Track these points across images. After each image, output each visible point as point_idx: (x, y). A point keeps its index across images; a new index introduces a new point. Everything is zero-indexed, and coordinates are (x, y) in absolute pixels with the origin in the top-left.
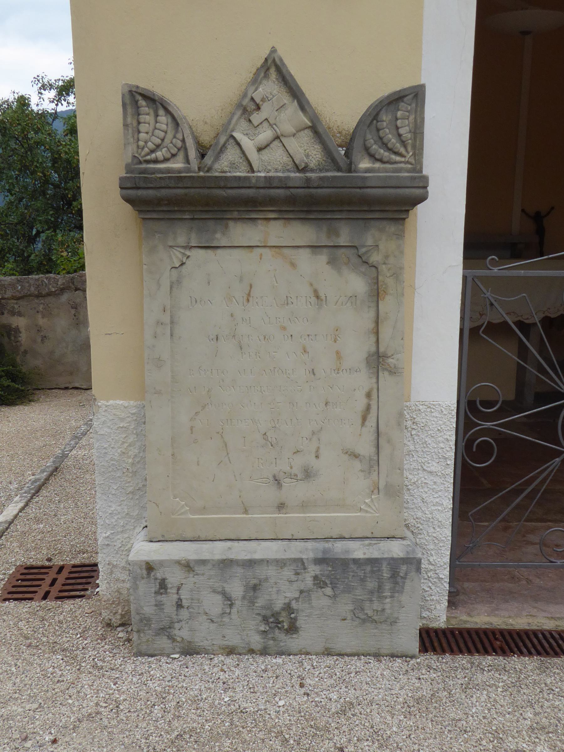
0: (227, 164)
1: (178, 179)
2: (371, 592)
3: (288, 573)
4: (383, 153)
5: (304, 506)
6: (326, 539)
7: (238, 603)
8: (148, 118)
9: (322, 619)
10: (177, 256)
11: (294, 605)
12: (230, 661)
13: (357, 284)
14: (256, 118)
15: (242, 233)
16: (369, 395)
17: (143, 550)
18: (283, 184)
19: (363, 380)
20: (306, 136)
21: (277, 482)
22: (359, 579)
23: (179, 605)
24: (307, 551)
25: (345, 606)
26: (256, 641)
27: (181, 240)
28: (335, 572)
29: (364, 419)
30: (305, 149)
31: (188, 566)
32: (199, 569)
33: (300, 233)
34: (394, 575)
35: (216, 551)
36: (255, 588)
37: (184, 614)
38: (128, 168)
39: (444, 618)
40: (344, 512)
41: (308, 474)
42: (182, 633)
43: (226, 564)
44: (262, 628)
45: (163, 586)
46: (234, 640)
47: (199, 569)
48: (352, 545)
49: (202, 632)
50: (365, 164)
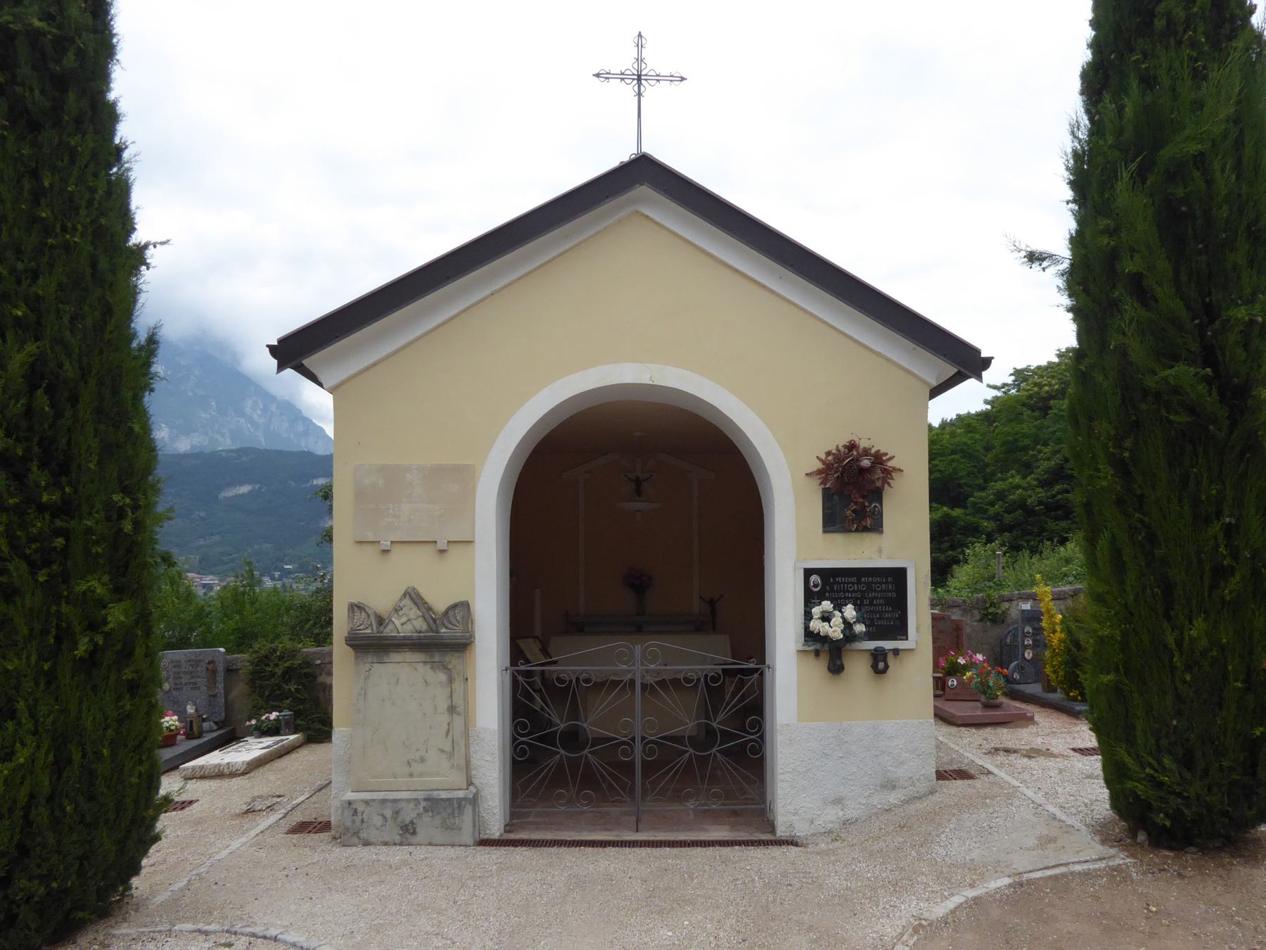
0: (389, 631)
1: (368, 637)
3: (412, 805)
5: (421, 775)
9: (428, 827)
10: (368, 665)
13: (442, 677)
15: (395, 657)
17: (350, 796)
18: (409, 638)
19: (445, 718)
20: (421, 619)
22: (446, 811)
23: (362, 821)
24: (420, 795)
25: (438, 821)
26: (398, 839)
28: (433, 804)
30: (420, 624)
31: (367, 802)
33: (419, 657)
34: (459, 806)
35: (381, 795)
36: (397, 813)
37: (365, 825)
40: (443, 778)
41: (423, 760)
42: (363, 835)
43: (384, 801)
45: (356, 811)
46: (387, 839)
49: (372, 834)
50: (443, 630)
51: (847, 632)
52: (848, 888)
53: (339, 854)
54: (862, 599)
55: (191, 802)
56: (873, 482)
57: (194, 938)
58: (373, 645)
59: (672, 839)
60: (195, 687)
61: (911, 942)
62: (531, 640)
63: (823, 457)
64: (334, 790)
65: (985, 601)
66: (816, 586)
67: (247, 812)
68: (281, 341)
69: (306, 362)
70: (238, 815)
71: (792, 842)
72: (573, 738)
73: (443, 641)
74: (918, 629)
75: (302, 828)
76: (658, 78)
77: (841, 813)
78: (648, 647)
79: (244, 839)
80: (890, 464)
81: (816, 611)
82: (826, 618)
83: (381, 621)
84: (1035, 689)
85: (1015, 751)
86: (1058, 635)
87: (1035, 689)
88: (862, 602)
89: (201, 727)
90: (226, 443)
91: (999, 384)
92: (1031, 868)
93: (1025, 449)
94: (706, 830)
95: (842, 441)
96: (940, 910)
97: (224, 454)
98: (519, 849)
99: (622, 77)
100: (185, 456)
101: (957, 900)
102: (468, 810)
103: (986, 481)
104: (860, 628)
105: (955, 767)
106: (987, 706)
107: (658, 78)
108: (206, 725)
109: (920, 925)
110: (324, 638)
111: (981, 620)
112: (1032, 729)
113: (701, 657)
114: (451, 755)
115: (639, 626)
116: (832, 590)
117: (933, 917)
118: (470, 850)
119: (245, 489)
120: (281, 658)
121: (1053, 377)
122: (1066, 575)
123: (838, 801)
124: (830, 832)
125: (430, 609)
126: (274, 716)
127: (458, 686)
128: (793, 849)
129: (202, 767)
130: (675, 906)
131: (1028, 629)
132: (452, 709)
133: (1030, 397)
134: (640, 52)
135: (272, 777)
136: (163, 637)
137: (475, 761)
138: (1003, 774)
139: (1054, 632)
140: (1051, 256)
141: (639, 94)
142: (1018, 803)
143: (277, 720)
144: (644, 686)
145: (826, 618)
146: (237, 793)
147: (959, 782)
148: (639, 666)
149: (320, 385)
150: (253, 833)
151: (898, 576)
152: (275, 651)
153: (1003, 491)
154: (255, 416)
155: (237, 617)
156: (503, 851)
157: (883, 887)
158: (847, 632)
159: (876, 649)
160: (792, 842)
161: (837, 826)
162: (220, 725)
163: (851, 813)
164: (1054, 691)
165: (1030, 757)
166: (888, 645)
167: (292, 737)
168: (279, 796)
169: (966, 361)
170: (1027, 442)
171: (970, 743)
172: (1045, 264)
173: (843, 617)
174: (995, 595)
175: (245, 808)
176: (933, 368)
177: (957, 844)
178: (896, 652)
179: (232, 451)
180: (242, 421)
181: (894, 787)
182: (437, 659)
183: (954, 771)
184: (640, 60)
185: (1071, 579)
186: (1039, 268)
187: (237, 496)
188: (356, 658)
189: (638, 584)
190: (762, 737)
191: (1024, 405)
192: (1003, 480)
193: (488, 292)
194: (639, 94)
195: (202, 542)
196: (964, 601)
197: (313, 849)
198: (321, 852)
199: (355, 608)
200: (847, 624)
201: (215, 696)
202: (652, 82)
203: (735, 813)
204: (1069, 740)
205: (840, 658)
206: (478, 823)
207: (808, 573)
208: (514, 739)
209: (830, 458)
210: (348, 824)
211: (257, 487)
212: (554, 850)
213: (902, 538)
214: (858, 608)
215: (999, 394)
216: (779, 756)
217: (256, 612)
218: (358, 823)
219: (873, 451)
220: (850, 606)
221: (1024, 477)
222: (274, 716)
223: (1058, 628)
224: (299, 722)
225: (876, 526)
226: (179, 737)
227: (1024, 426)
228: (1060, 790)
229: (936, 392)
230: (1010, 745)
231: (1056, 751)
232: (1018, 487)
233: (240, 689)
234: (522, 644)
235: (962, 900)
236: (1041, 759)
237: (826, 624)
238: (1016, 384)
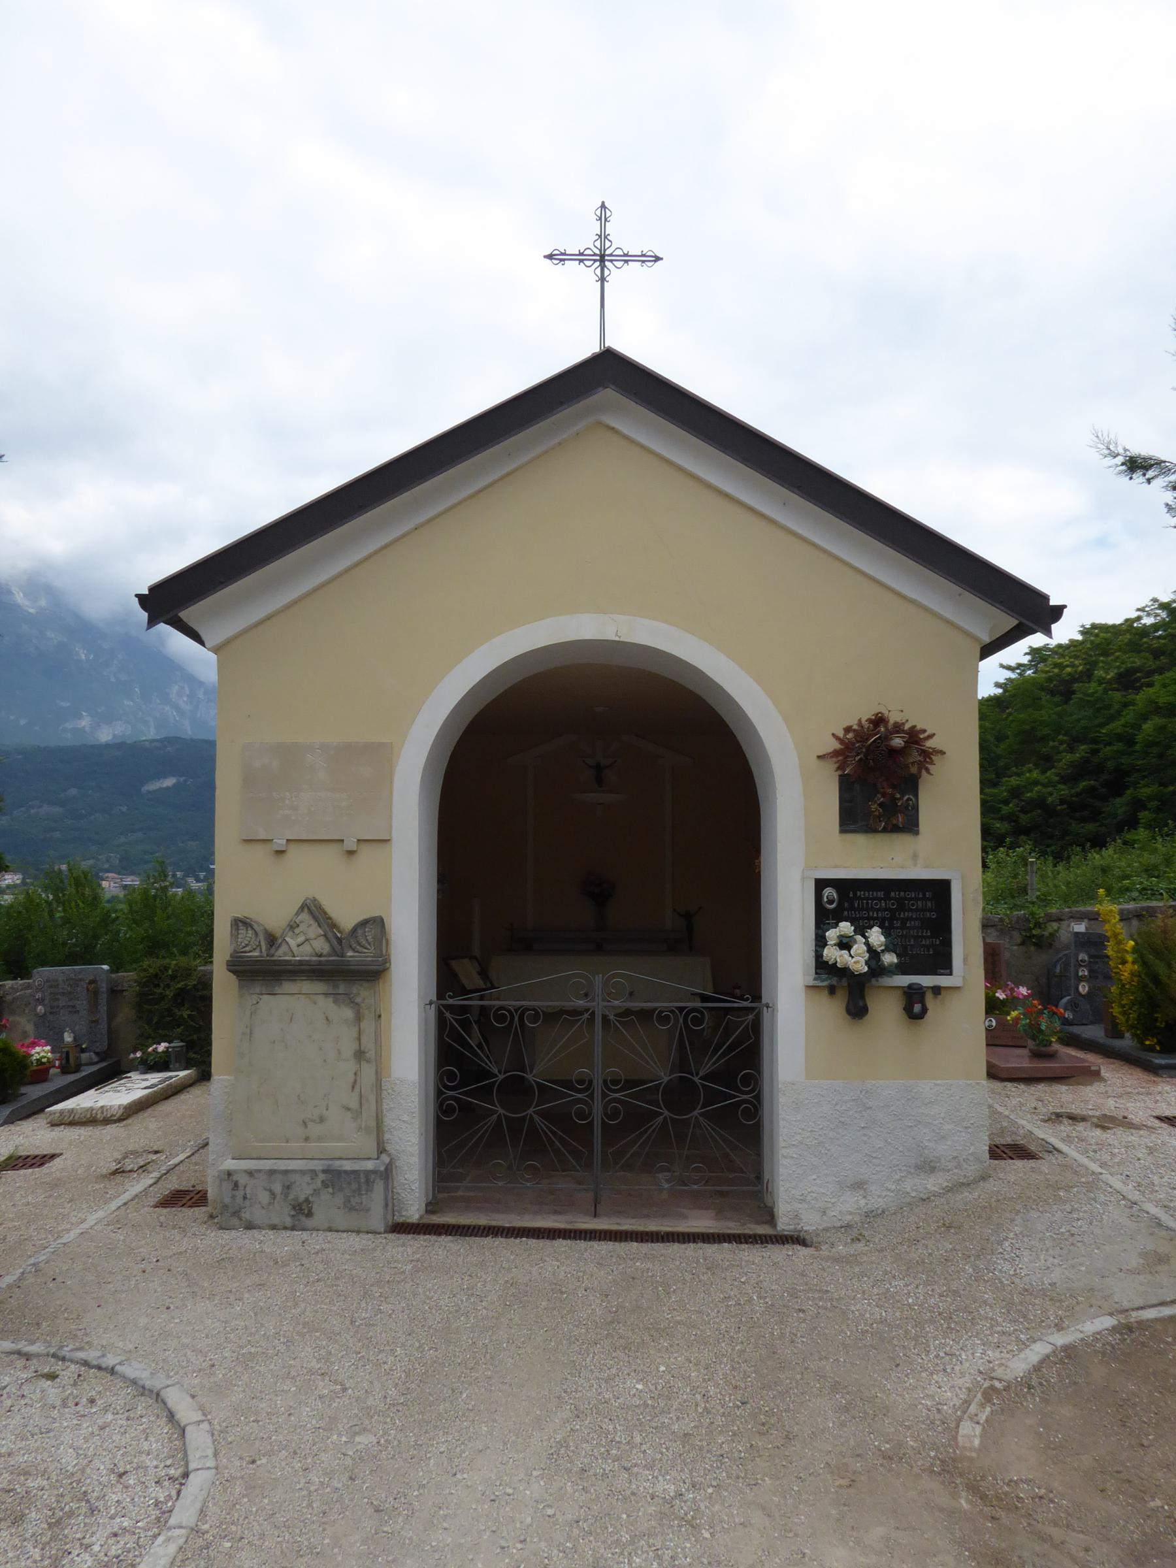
0: (281, 954)
2: (354, 1191)
3: (307, 1178)
4: (360, 949)
5: (320, 1139)
6: (332, 1159)
7: (278, 1197)
8: (242, 931)
9: (327, 1207)
10: (255, 997)
11: (311, 1199)
12: (271, 1232)
13: (349, 1013)
14: (297, 931)
15: (289, 987)
16: (355, 1074)
17: (230, 1164)
18: (308, 963)
19: (351, 1066)
21: (305, 1124)
23: (245, 1198)
24: (318, 1165)
25: (339, 1199)
26: (288, 1221)
27: (258, 990)
28: (334, 1178)
29: (353, 1087)
30: (321, 946)
31: (250, 1173)
32: (256, 1175)
33: (319, 987)
34: (367, 1181)
36: (288, 1187)
37: (247, 1203)
38: (231, 956)
39: (417, 1216)
40: (349, 1145)
41: (322, 1119)
42: (246, 1215)
43: (272, 1172)
44: (293, 1213)
45: (236, 1185)
46: (276, 1221)
47: (256, 1175)
48: (345, 1162)
49: (255, 1213)
50: (350, 954)
51: (873, 963)
52: (882, 1321)
53: (216, 1240)
54: (891, 920)
55: (53, 1157)
56: (907, 766)
57: (11, 1364)
58: (262, 971)
59: (641, 1228)
60: (74, 1010)
61: (982, 1418)
62: (466, 961)
63: (841, 734)
64: (211, 1153)
65: (1027, 920)
66: (831, 902)
67: (116, 1172)
68: (152, 589)
69: (183, 615)
70: (104, 1176)
71: (797, 1239)
72: (516, 1089)
73: (348, 967)
74: (965, 960)
75: (176, 1199)
76: (627, 258)
77: (862, 1202)
78: (614, 976)
79: (101, 1214)
80: (930, 744)
81: (832, 935)
82: (845, 944)
83: (272, 940)
84: (1094, 1032)
85: (1084, 1119)
86: (1129, 966)
87: (1094, 1032)
88: (891, 923)
89: (78, 1058)
90: (150, 734)
91: (1013, 664)
92: (1140, 1302)
93: (1044, 739)
94: (685, 1217)
95: (866, 714)
96: (1020, 1364)
97: (147, 744)
98: (445, 1240)
99: (581, 257)
100: (108, 746)
101: (1040, 1350)
102: (379, 1187)
103: (999, 776)
104: (890, 959)
105: (1008, 1140)
106: (1037, 1055)
107: (627, 258)
108: (84, 1057)
109: (992, 1388)
110: (209, 960)
111: (1023, 944)
112: (1098, 1087)
113: (675, 985)
114: (357, 1114)
115: (599, 943)
116: (852, 908)
117: (1009, 1376)
118: (381, 1239)
119: (169, 782)
120: (173, 977)
121: (1076, 657)
122: (1127, 890)
123: (859, 1185)
124: (848, 1226)
125: (333, 926)
126: (162, 1047)
127: (368, 1025)
128: (802, 1251)
129: (72, 1111)
130: (647, 1338)
131: (1083, 956)
132: (360, 1055)
133: (1050, 680)
134: (603, 228)
135: (153, 1126)
136: (64, 944)
137: (389, 1121)
138: (1074, 1154)
139: (1124, 962)
140: (1159, 463)
141: (603, 280)
142: (1102, 1198)
143: (166, 1052)
144: (605, 1018)
145: (845, 944)
146: (108, 1145)
147: (1019, 1164)
148: (600, 1007)
149: (202, 643)
150: (113, 1205)
151: (940, 890)
152: (166, 969)
153: (1019, 787)
154: (181, 703)
155: (147, 924)
156: (422, 1240)
157: (932, 1321)
158: (873, 963)
159: (910, 986)
160: (797, 1239)
161: (857, 1218)
162: (103, 1056)
163: (878, 1199)
164: (1121, 1036)
165: (1104, 1128)
166: (926, 981)
167: (182, 1074)
168: (156, 1152)
169: (1030, 609)
170: (1046, 731)
171: (1021, 1105)
172: (1150, 474)
173: (867, 944)
174: (1040, 913)
175: (114, 1166)
176: (985, 619)
177: (1030, 1260)
178: (937, 990)
179: (157, 741)
180: (167, 708)
181: (933, 1170)
182: (341, 990)
183: (1008, 1146)
184: (603, 236)
185: (1135, 894)
186: (1142, 479)
187: (161, 789)
188: (241, 987)
189: (599, 893)
190: (758, 1098)
191: (1042, 688)
192: (1018, 775)
193: (411, 526)
194: (603, 280)
195: (123, 839)
196: (1001, 920)
197: (184, 1231)
198: (195, 1237)
199: (240, 923)
200: (874, 954)
201: (96, 1022)
202: (619, 264)
203: (721, 1194)
204: (1150, 1104)
205: (863, 997)
206: (391, 1202)
207: (821, 884)
208: (439, 1093)
209: (850, 736)
210: (227, 1200)
211: (182, 779)
212: (488, 1241)
213: (946, 842)
214: (886, 932)
215: (1013, 676)
216: (782, 1123)
217: (168, 918)
218: (239, 1200)
219: (907, 727)
220: (876, 929)
221: (1044, 772)
222: (162, 1047)
223: (1130, 958)
224: (191, 1055)
225: (911, 826)
226: (53, 1071)
227: (1043, 712)
228: (1156, 1180)
229: (988, 650)
230: (1073, 1109)
231: (1135, 1119)
232: (1036, 783)
233: (126, 1013)
234: (456, 965)
235: (1048, 1349)
236: (1119, 1131)
237: (845, 952)
238: (1033, 664)
